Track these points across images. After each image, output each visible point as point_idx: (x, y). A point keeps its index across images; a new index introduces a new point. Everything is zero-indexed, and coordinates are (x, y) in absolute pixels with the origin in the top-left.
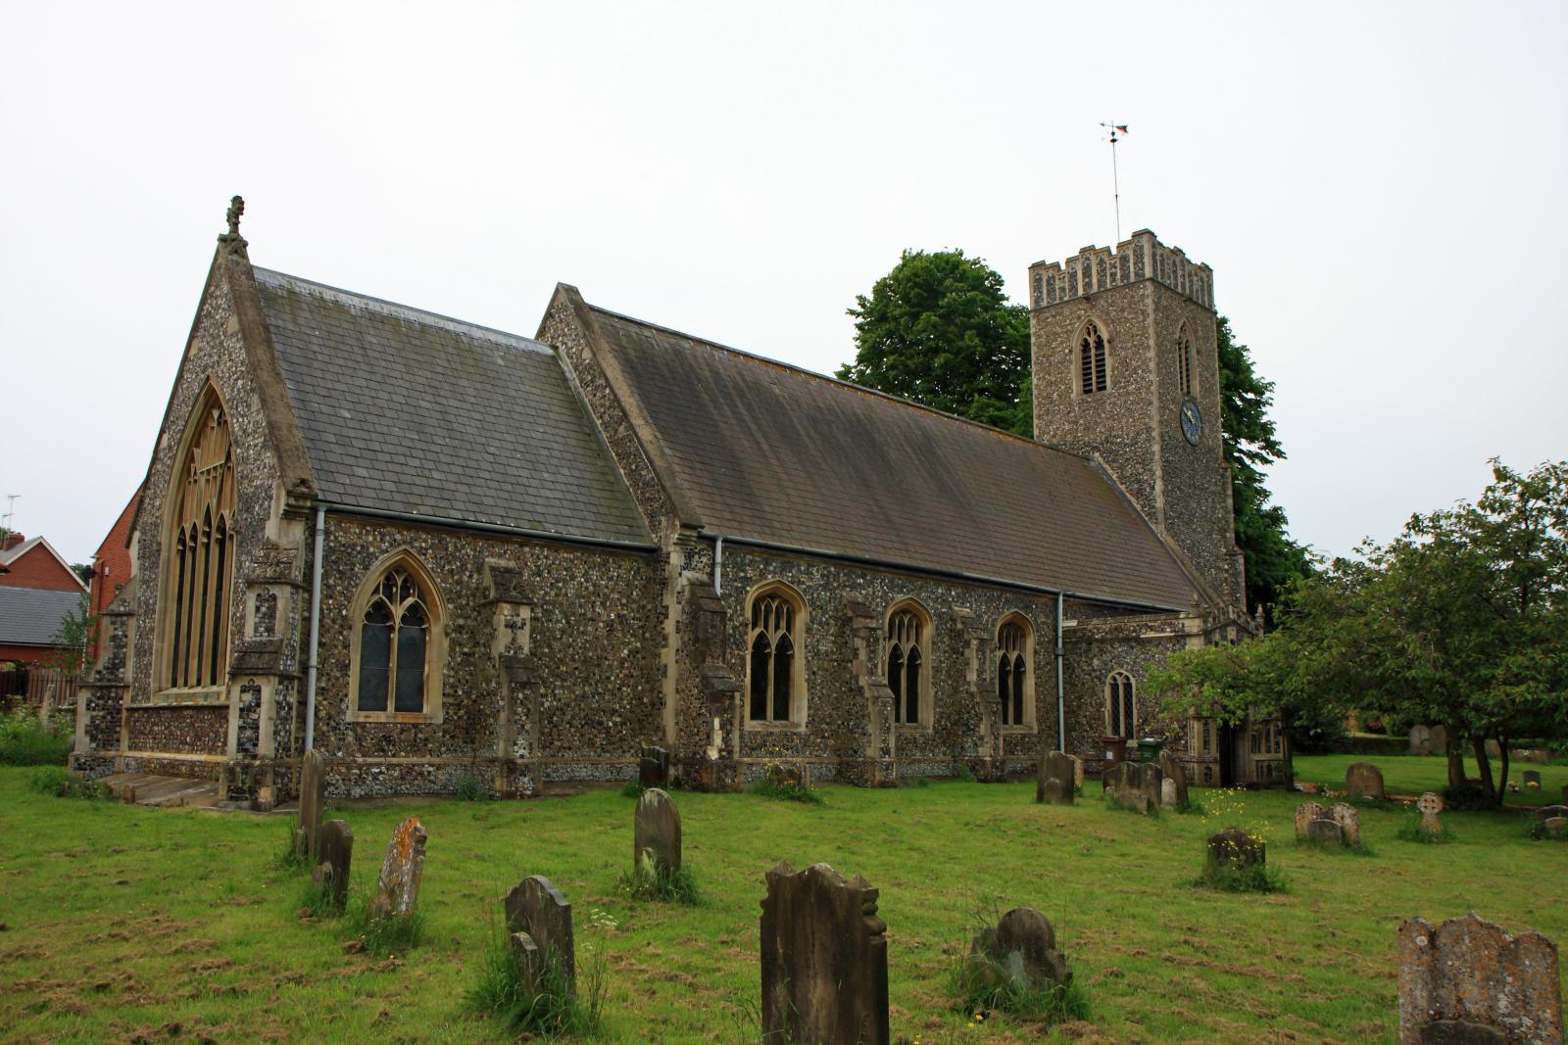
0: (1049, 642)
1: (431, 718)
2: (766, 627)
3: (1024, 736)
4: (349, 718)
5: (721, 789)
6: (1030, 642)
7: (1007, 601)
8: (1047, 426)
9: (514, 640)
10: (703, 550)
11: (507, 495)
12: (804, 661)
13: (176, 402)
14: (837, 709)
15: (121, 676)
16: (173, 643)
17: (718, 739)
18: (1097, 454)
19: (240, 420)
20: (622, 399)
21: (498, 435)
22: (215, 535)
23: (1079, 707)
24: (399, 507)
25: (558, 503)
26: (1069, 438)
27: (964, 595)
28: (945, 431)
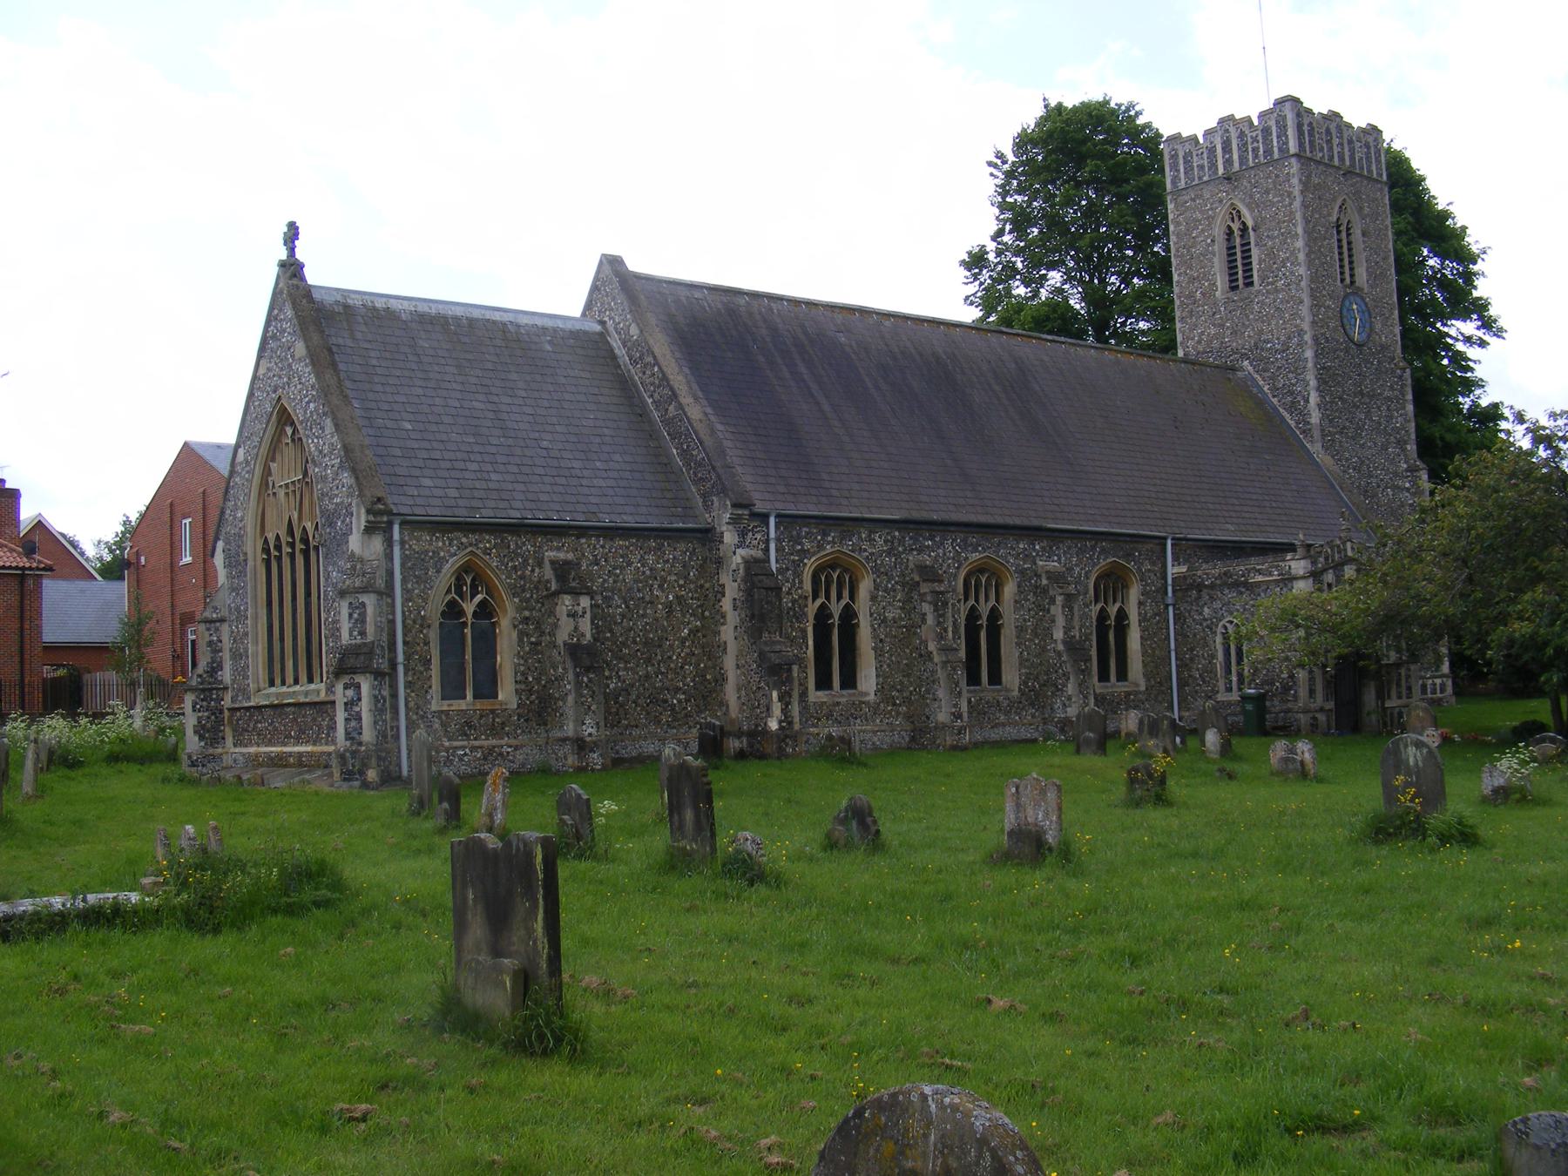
0: (1157, 591)
1: (506, 704)
2: (828, 597)
3: (1128, 694)
4: (434, 707)
5: (781, 755)
6: (1134, 593)
7: (1103, 550)
8: (1192, 330)
9: (576, 628)
10: (756, 527)
11: (561, 489)
12: (869, 629)
13: (248, 418)
14: (908, 675)
15: (220, 678)
16: (266, 645)
17: (777, 709)
18: (1246, 363)
19: (316, 441)
20: (671, 377)
21: (549, 428)
22: (299, 546)
23: (1192, 659)
24: (464, 512)
25: (611, 492)
26: (1216, 344)
27: (1051, 548)
28: (1046, 358)
